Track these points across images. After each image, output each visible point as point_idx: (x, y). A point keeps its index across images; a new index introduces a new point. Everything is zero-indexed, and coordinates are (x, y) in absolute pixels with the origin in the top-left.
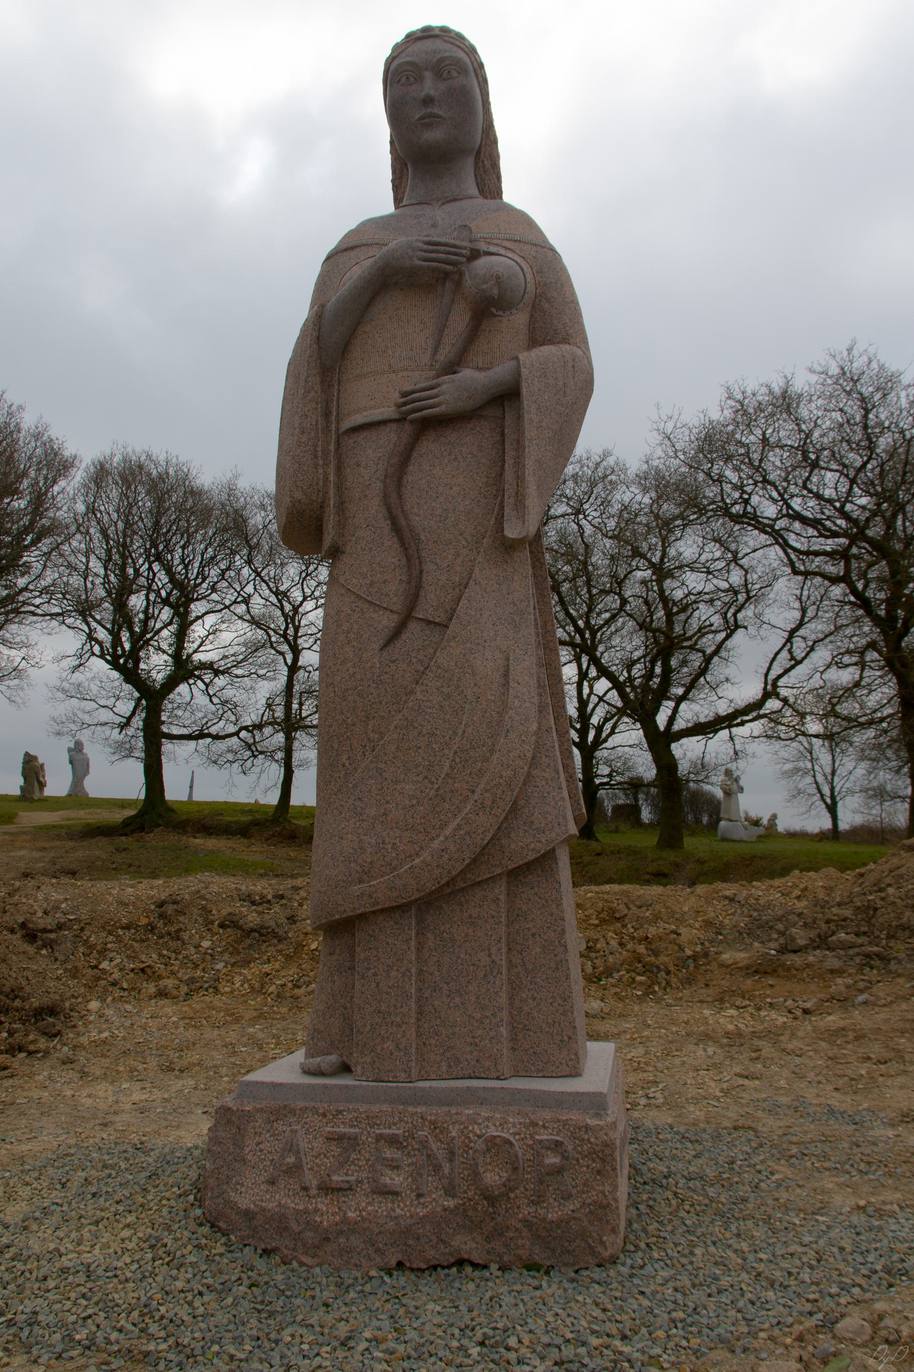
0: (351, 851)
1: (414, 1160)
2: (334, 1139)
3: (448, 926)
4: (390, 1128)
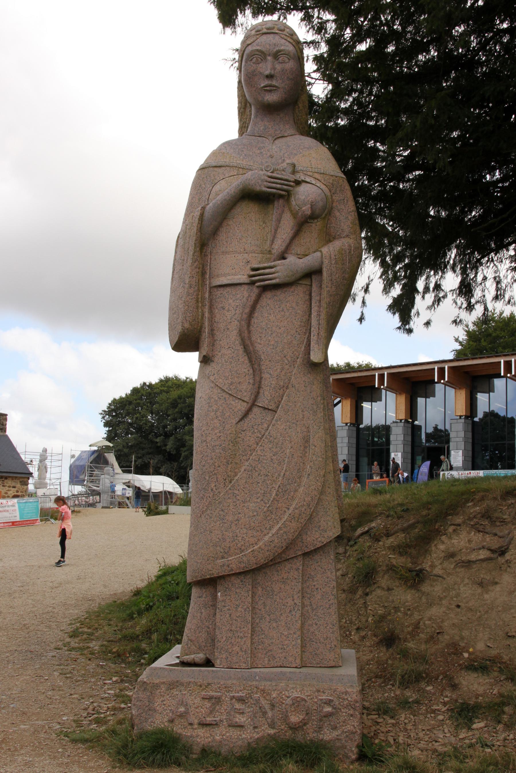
0: (217, 540)
1: (252, 709)
2: (207, 699)
3: (270, 583)
4: (238, 693)
